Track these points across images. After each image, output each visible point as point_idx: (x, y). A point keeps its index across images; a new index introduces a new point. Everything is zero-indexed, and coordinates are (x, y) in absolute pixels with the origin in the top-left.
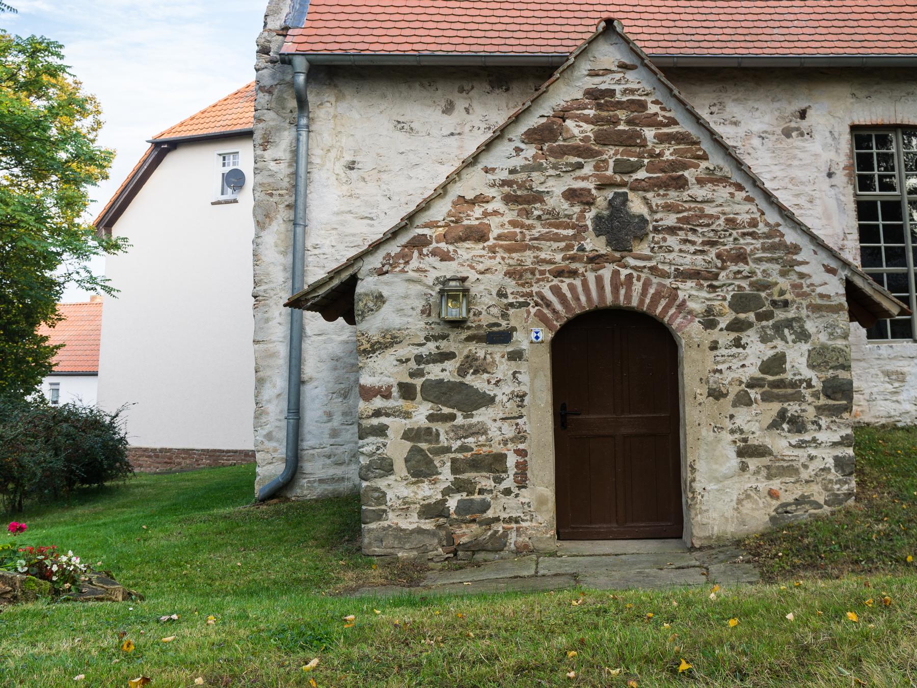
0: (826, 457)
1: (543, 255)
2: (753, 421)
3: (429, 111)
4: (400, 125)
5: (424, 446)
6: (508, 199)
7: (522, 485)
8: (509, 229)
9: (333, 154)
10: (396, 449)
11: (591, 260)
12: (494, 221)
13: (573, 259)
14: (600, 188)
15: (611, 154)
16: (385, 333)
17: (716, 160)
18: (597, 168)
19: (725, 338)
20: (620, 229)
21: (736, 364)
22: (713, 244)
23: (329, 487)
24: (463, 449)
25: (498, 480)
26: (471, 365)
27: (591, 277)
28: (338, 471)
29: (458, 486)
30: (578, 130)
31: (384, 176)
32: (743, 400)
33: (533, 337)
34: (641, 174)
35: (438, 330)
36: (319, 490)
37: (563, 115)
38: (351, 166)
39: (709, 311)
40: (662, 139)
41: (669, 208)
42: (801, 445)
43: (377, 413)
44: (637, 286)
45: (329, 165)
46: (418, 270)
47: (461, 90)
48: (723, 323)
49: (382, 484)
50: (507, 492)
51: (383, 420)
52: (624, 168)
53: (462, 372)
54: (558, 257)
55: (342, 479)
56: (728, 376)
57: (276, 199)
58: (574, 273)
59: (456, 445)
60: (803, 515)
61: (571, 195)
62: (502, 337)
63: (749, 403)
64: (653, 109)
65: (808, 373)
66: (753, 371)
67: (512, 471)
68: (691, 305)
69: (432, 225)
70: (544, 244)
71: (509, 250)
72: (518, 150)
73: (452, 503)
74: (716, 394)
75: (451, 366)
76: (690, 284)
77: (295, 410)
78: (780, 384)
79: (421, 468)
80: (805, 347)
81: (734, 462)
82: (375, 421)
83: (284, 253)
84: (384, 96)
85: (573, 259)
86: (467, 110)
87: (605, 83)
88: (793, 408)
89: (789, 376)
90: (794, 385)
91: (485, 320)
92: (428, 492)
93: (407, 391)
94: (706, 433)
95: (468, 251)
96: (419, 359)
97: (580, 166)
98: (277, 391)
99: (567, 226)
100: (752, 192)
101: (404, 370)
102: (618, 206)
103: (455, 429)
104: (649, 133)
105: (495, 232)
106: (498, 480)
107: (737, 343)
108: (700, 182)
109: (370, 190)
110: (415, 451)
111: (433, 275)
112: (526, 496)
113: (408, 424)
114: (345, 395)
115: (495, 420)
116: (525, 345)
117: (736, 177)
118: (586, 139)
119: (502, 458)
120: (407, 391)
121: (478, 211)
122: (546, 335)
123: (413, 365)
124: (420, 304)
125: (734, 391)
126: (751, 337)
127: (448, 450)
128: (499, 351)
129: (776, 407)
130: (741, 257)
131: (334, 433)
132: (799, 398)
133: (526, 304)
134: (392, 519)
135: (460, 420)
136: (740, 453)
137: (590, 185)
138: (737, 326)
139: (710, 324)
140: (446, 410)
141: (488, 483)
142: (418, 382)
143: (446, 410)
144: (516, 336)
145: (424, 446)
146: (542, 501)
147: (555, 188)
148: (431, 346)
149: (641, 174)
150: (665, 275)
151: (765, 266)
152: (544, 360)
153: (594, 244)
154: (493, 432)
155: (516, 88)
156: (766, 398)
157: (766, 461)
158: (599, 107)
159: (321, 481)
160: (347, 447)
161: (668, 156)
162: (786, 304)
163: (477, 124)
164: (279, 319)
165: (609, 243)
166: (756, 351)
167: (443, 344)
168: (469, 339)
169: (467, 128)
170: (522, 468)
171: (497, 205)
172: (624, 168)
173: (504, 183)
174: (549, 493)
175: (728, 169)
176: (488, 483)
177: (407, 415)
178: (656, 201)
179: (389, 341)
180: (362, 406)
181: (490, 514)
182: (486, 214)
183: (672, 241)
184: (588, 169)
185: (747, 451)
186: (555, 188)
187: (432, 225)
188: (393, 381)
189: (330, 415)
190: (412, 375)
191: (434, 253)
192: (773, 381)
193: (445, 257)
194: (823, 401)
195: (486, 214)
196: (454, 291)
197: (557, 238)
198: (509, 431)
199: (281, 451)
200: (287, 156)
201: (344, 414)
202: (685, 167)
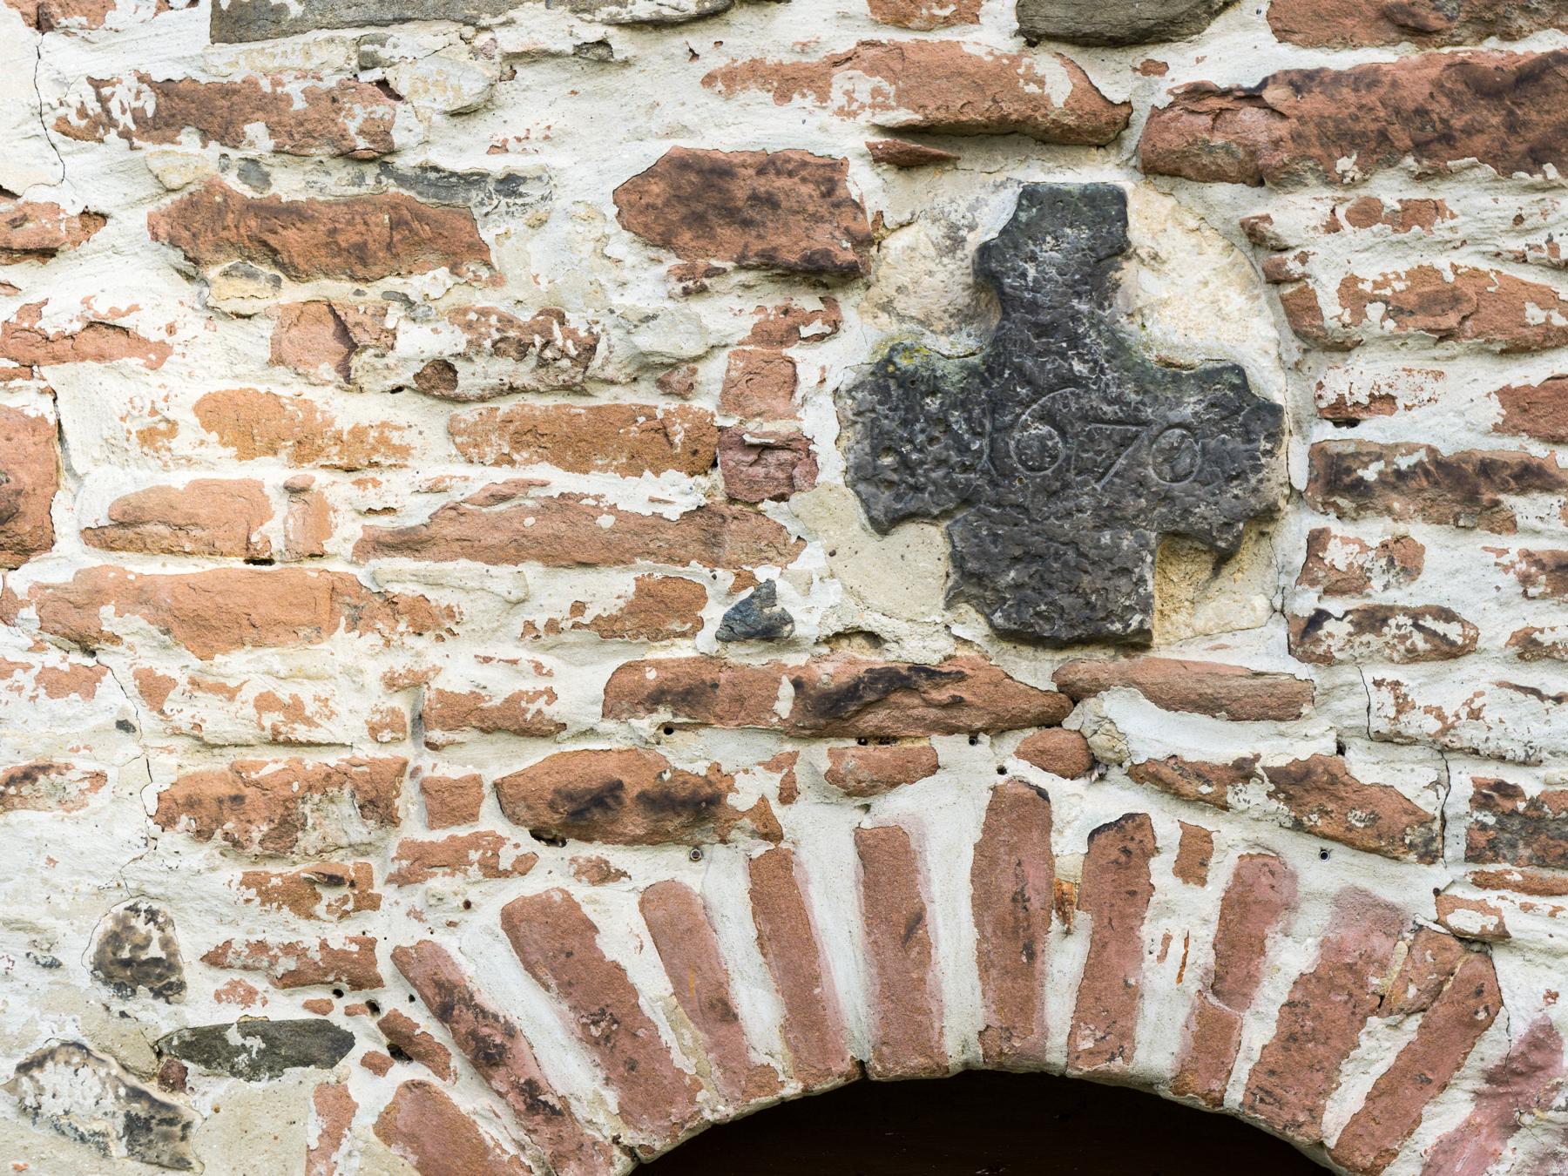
1: (456, 670)
6: (201, 232)
13: (690, 699)
14: (917, 148)
20: (1056, 473)
27: (824, 840)
41: (1441, 314)
44: (1182, 917)
54: (578, 684)
58: (691, 811)
61: (693, 205)
70: (460, 581)
85: (690, 699)
99: (650, 449)
137: (838, 130)
150: (1398, 835)
153: (869, 584)
165: (970, 581)
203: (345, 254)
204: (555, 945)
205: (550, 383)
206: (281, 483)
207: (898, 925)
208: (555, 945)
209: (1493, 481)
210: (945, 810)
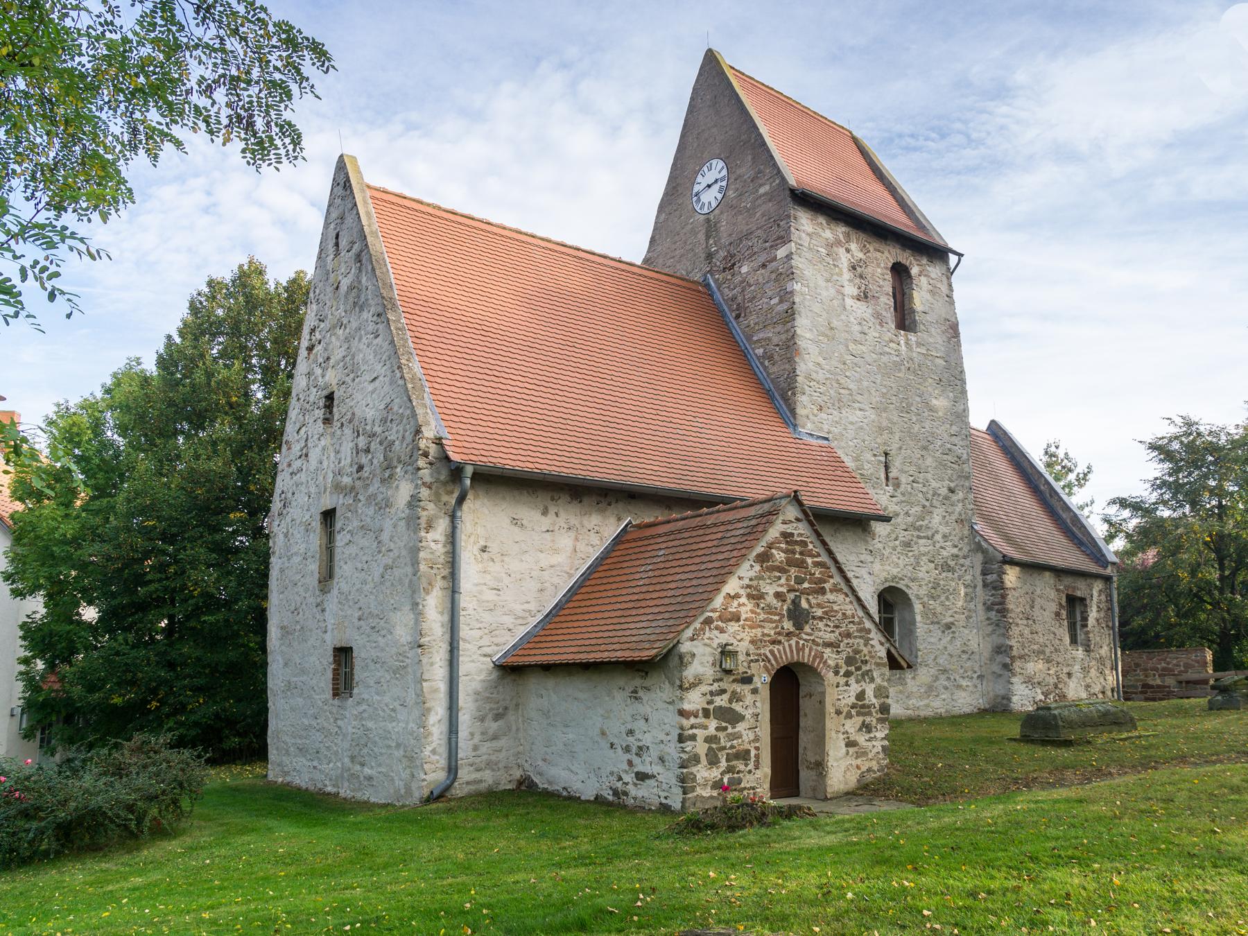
0: (878, 745)
1: (766, 631)
2: (852, 726)
3: (533, 513)
4: (515, 521)
5: (714, 746)
6: (749, 596)
7: (757, 768)
8: (750, 615)
9: (472, 539)
10: (701, 748)
11: (787, 635)
12: (743, 609)
13: (779, 634)
14: (789, 591)
15: (793, 571)
16: (695, 677)
17: (837, 579)
18: (787, 580)
19: (842, 681)
20: (799, 617)
21: (846, 695)
22: (837, 627)
23: (473, 787)
24: (732, 747)
25: (746, 765)
26: (736, 697)
27: (786, 644)
28: (478, 775)
29: (730, 770)
30: (779, 556)
31: (506, 559)
32: (849, 716)
33: (762, 679)
34: (806, 585)
35: (719, 675)
36: (467, 789)
37: (770, 546)
38: (484, 549)
39: (837, 666)
40: (816, 564)
41: (819, 605)
42: (869, 740)
43: (692, 727)
44: (807, 650)
45: (470, 547)
46: (710, 639)
47: (553, 499)
48: (842, 672)
49: (694, 770)
50: (750, 772)
51: (694, 731)
52: (799, 581)
53: (730, 701)
54: (772, 633)
55: (481, 781)
56: (843, 702)
57: (434, 571)
58: (780, 642)
59: (728, 745)
60: (870, 777)
61: (778, 595)
62: (747, 680)
63: (851, 717)
64: (810, 546)
65: (874, 701)
66: (853, 700)
67: (753, 759)
68: (830, 662)
69: (713, 611)
70: (766, 624)
71: (751, 627)
72: (752, 566)
73: (725, 780)
74: (838, 713)
75: (726, 697)
76: (828, 650)
77: (453, 729)
78: (863, 706)
79: (713, 762)
80: (873, 686)
81: (844, 750)
82: (691, 732)
83: (442, 613)
84: (504, 498)
85: (779, 634)
86: (557, 514)
87: (789, 529)
88: (868, 719)
89: (866, 702)
90: (869, 707)
91: (741, 670)
92: (715, 774)
93: (706, 713)
94: (833, 734)
95: (733, 627)
96: (712, 693)
97: (780, 578)
98: (439, 717)
99: (776, 614)
100: (852, 598)
101: (704, 700)
102: (796, 603)
103: (728, 735)
104: (809, 560)
105: (743, 616)
106: (746, 765)
107: (847, 684)
108: (831, 591)
109: (495, 568)
110: (710, 749)
111: (716, 641)
112: (759, 774)
113: (707, 733)
114: (482, 719)
115: (603, 734)
116: (759, 685)
117: (846, 589)
118: (781, 562)
119: (748, 752)
120: (706, 713)
121: (735, 603)
122: (768, 679)
123: (708, 697)
124: (711, 659)
125: (845, 710)
126: (852, 680)
127: (724, 748)
128: (747, 688)
129: (861, 719)
130: (848, 635)
131: (475, 748)
132: (870, 714)
133: (757, 661)
134: (699, 791)
135: (730, 730)
136: (847, 745)
137: (784, 590)
138: (848, 674)
139: (837, 673)
140: (724, 724)
141: (742, 767)
142: (711, 707)
143: (724, 724)
144: (755, 679)
145: (714, 746)
146: (765, 777)
147: (770, 589)
148: (716, 686)
149: (806, 585)
150: (818, 645)
151: (858, 640)
152: (765, 693)
153: (788, 625)
154: (745, 737)
155: (586, 500)
156: (858, 714)
157: (855, 749)
158: (787, 543)
159: (468, 783)
160: (484, 757)
161: (817, 575)
162: (866, 662)
163: (563, 525)
164: (440, 664)
165: (794, 625)
166: (855, 688)
167: (721, 684)
168: (734, 681)
169: (557, 528)
170: (757, 756)
171: (743, 600)
172: (799, 581)
173: (748, 586)
174: (768, 771)
175: (843, 586)
176: (742, 767)
177: (706, 728)
178: (813, 601)
179: (697, 682)
180: (685, 723)
181: (742, 785)
182: (739, 605)
183: (821, 625)
184: (783, 581)
185: (850, 744)
186: (770, 589)
187: (713, 611)
188: (699, 707)
189: (472, 734)
190: (708, 703)
191: (717, 628)
192: (860, 706)
193: (722, 631)
194: (880, 715)
195: (739, 605)
196: (726, 652)
197: (771, 621)
198: (752, 737)
199: (442, 762)
200: (442, 538)
201: (482, 733)
202: (825, 582)
203: (181, 405)
204: (772, 652)
205: (769, 610)
206: (261, 258)
207: (792, 651)
208: (772, 652)
209: (111, 407)
210: (793, 642)
